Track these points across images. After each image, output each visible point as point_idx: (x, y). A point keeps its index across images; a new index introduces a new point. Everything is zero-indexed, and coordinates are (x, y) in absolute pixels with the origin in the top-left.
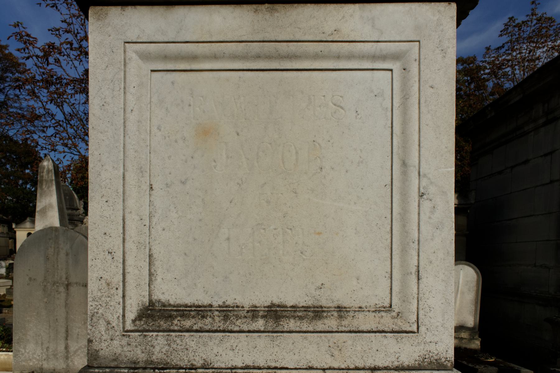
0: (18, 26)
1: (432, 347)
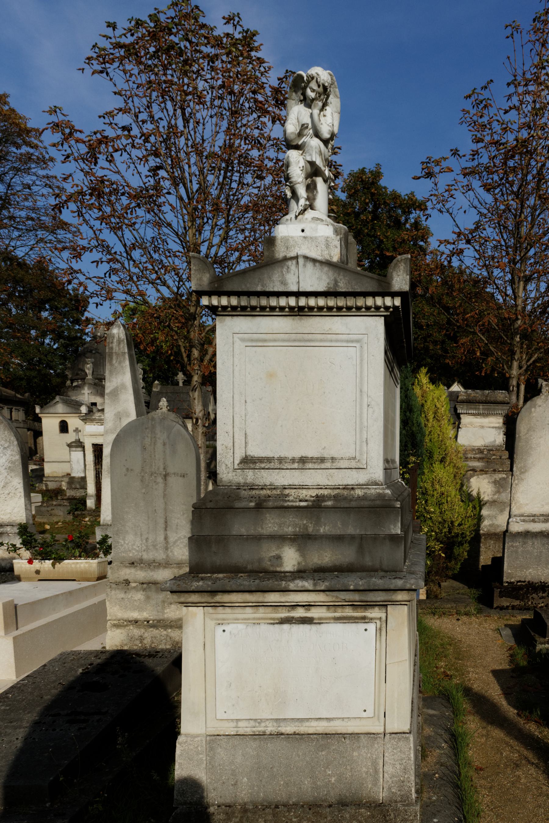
0: (56, 112)
1: (373, 475)
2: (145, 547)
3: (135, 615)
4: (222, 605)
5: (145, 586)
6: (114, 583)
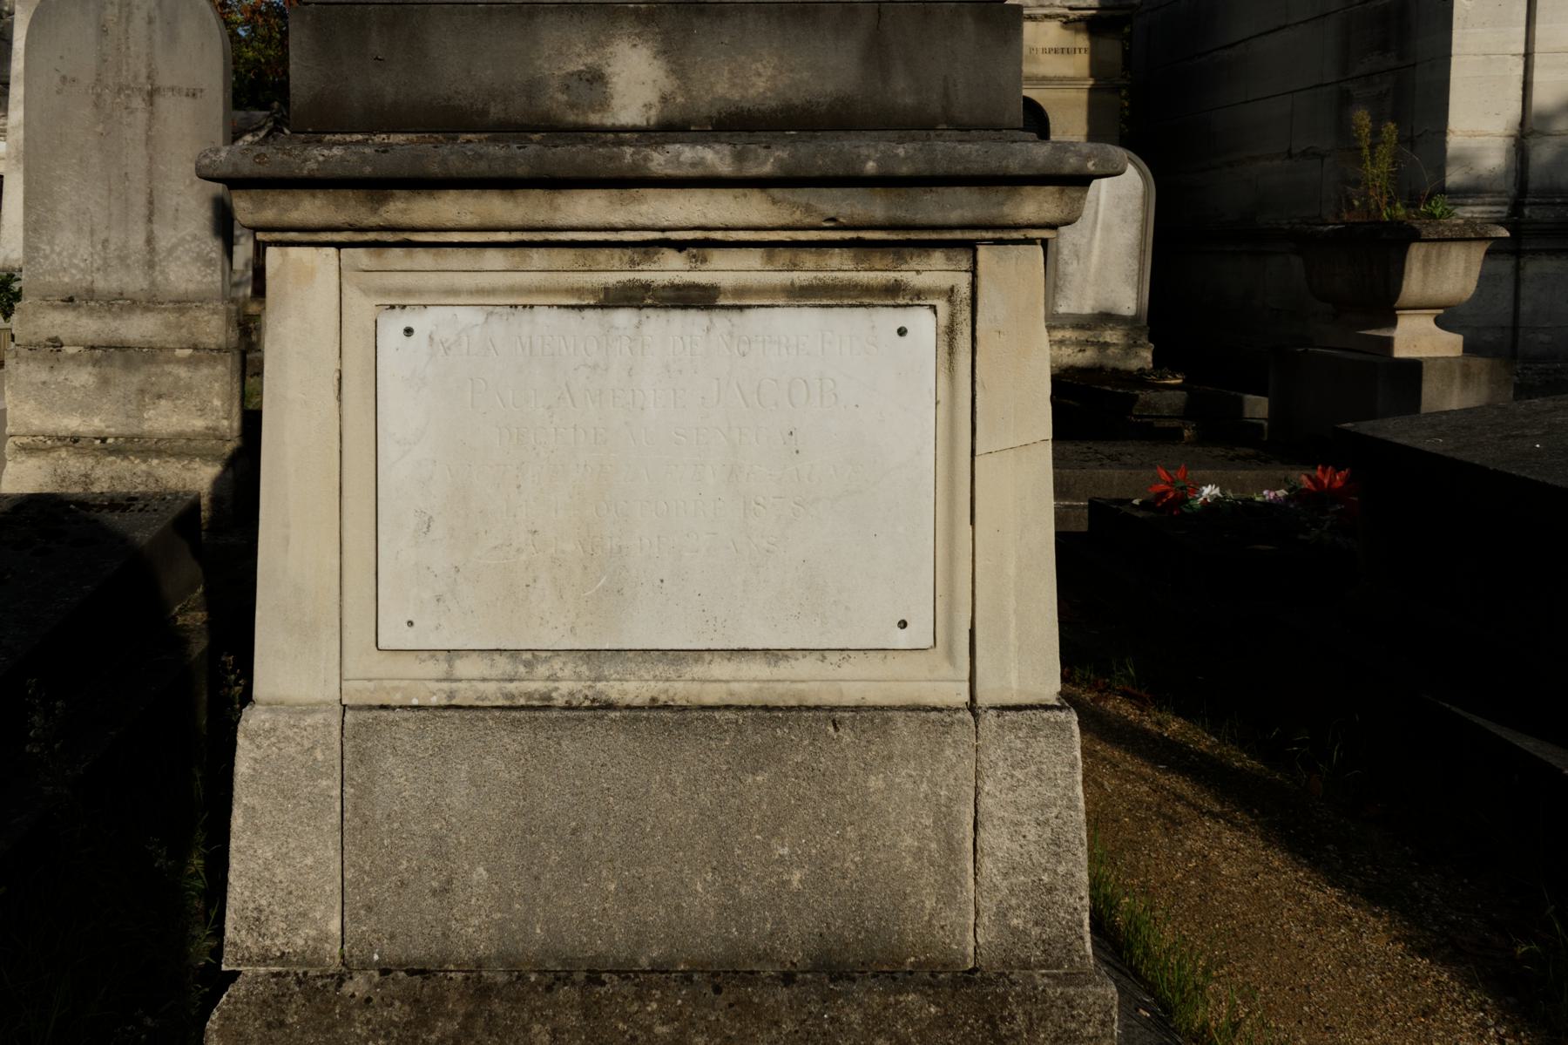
2: (100, 262)
3: (73, 423)
4: (405, 239)
5: (98, 352)
6: (25, 346)
